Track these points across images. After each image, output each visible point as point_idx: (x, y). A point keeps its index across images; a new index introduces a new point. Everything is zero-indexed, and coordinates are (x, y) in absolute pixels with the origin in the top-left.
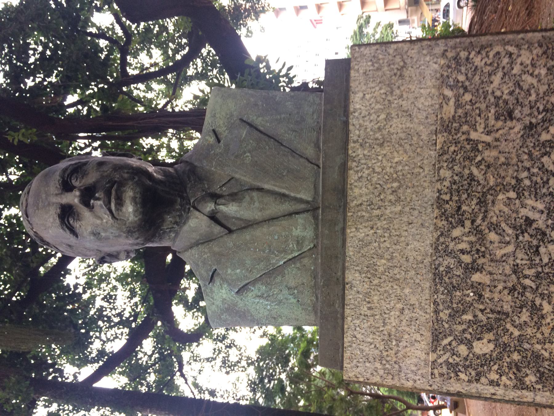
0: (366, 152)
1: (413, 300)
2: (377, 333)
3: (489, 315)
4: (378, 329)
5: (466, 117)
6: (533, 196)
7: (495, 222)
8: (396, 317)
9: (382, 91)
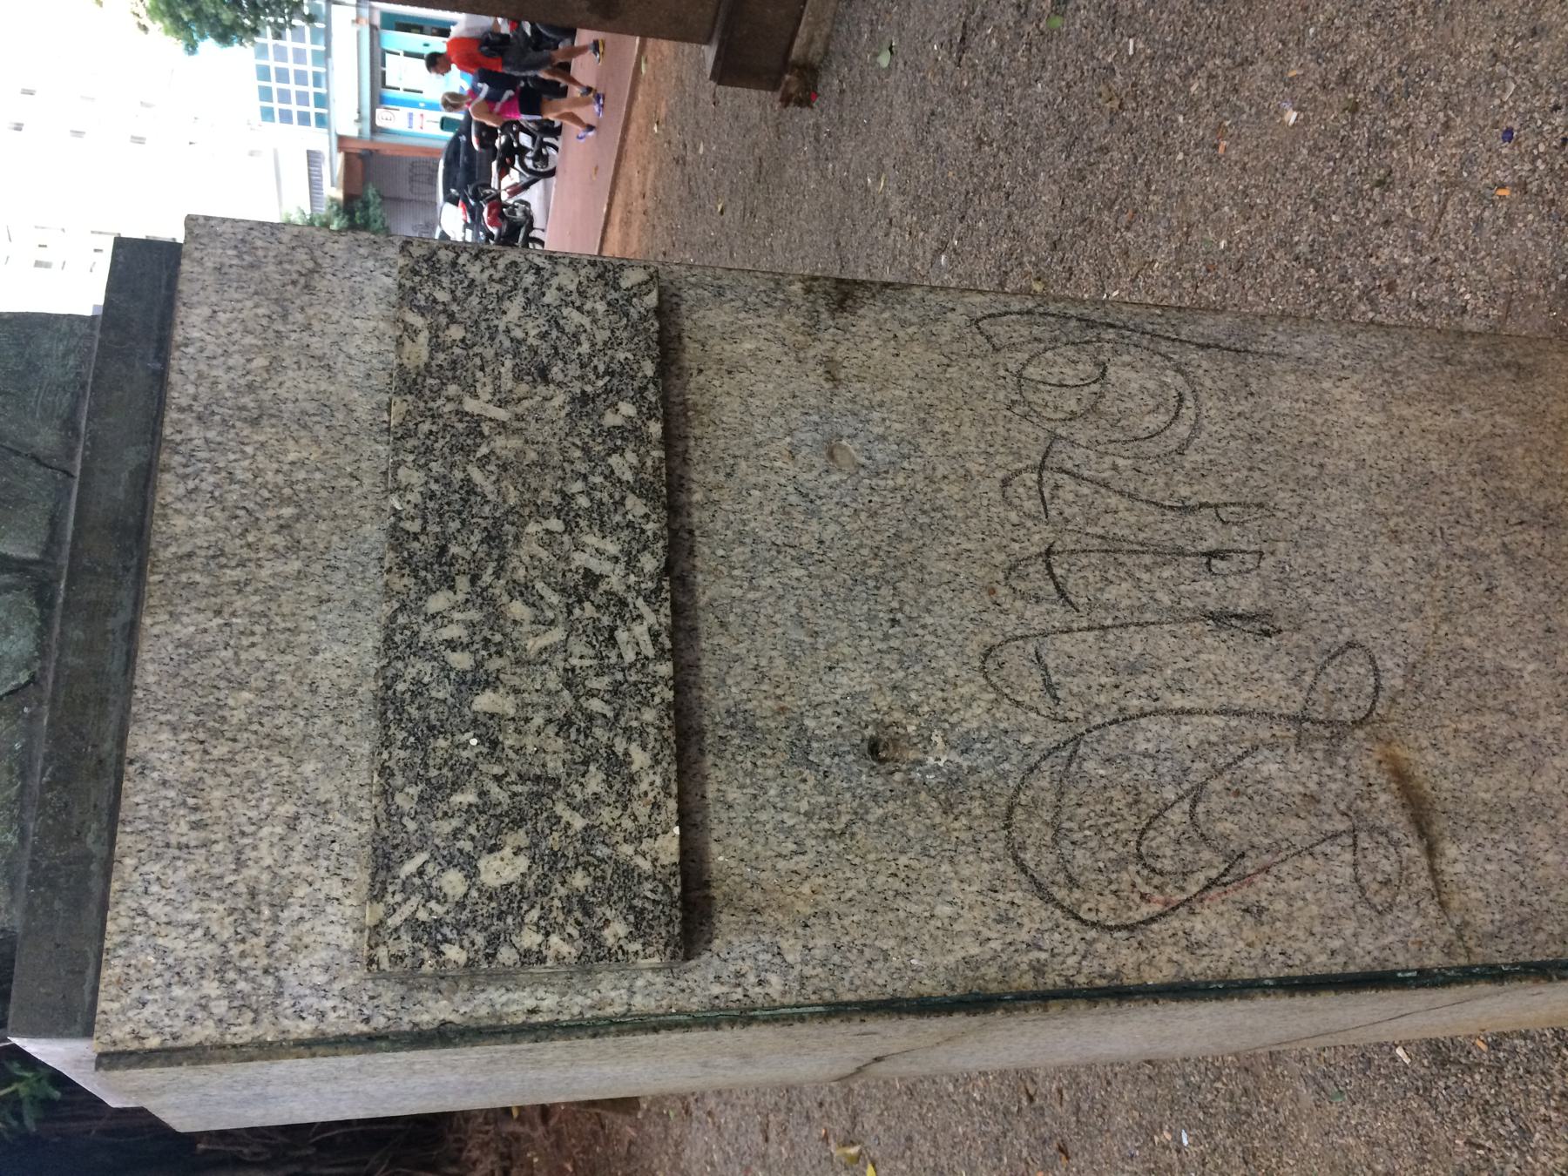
0: (211, 435)
1: (326, 791)
2: (215, 894)
3: (515, 788)
4: (218, 883)
5: (454, 369)
6: (596, 529)
7: (523, 580)
8: (275, 840)
9: (261, 311)
